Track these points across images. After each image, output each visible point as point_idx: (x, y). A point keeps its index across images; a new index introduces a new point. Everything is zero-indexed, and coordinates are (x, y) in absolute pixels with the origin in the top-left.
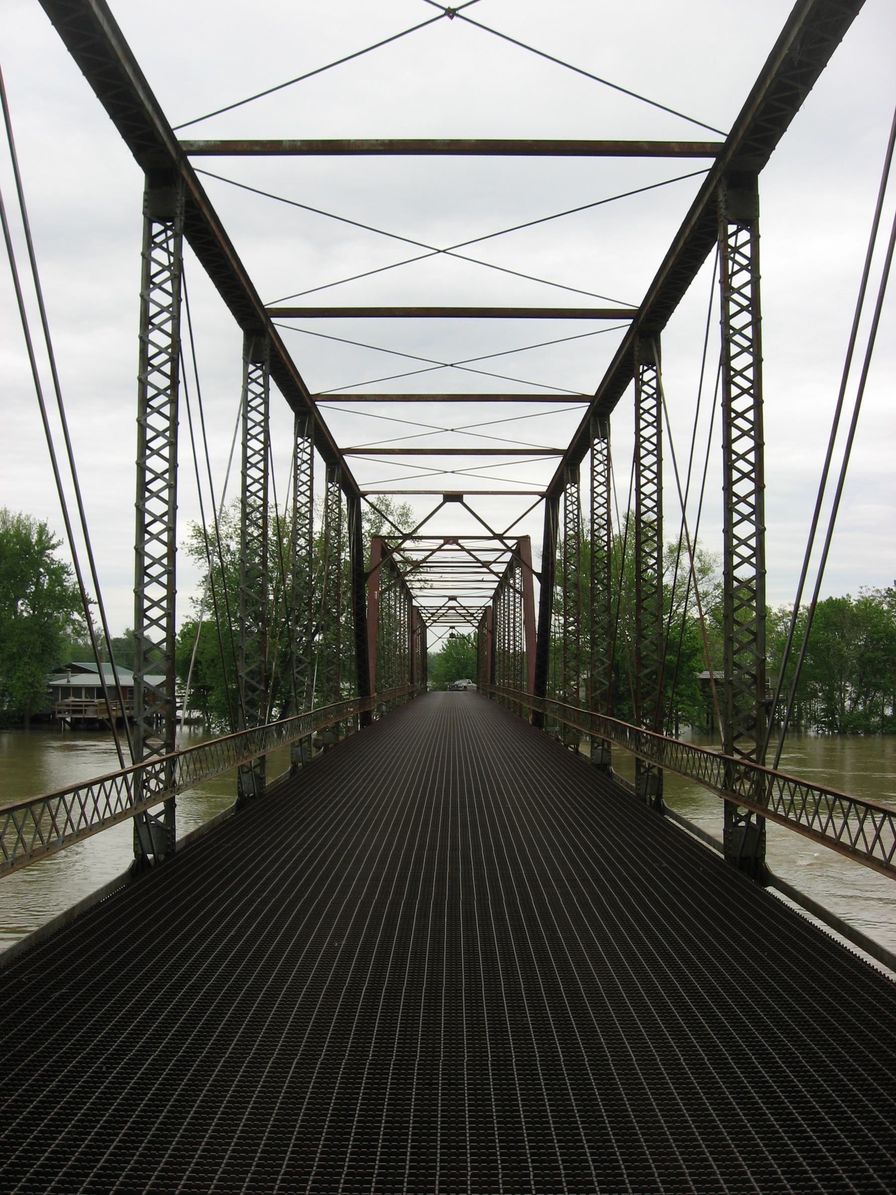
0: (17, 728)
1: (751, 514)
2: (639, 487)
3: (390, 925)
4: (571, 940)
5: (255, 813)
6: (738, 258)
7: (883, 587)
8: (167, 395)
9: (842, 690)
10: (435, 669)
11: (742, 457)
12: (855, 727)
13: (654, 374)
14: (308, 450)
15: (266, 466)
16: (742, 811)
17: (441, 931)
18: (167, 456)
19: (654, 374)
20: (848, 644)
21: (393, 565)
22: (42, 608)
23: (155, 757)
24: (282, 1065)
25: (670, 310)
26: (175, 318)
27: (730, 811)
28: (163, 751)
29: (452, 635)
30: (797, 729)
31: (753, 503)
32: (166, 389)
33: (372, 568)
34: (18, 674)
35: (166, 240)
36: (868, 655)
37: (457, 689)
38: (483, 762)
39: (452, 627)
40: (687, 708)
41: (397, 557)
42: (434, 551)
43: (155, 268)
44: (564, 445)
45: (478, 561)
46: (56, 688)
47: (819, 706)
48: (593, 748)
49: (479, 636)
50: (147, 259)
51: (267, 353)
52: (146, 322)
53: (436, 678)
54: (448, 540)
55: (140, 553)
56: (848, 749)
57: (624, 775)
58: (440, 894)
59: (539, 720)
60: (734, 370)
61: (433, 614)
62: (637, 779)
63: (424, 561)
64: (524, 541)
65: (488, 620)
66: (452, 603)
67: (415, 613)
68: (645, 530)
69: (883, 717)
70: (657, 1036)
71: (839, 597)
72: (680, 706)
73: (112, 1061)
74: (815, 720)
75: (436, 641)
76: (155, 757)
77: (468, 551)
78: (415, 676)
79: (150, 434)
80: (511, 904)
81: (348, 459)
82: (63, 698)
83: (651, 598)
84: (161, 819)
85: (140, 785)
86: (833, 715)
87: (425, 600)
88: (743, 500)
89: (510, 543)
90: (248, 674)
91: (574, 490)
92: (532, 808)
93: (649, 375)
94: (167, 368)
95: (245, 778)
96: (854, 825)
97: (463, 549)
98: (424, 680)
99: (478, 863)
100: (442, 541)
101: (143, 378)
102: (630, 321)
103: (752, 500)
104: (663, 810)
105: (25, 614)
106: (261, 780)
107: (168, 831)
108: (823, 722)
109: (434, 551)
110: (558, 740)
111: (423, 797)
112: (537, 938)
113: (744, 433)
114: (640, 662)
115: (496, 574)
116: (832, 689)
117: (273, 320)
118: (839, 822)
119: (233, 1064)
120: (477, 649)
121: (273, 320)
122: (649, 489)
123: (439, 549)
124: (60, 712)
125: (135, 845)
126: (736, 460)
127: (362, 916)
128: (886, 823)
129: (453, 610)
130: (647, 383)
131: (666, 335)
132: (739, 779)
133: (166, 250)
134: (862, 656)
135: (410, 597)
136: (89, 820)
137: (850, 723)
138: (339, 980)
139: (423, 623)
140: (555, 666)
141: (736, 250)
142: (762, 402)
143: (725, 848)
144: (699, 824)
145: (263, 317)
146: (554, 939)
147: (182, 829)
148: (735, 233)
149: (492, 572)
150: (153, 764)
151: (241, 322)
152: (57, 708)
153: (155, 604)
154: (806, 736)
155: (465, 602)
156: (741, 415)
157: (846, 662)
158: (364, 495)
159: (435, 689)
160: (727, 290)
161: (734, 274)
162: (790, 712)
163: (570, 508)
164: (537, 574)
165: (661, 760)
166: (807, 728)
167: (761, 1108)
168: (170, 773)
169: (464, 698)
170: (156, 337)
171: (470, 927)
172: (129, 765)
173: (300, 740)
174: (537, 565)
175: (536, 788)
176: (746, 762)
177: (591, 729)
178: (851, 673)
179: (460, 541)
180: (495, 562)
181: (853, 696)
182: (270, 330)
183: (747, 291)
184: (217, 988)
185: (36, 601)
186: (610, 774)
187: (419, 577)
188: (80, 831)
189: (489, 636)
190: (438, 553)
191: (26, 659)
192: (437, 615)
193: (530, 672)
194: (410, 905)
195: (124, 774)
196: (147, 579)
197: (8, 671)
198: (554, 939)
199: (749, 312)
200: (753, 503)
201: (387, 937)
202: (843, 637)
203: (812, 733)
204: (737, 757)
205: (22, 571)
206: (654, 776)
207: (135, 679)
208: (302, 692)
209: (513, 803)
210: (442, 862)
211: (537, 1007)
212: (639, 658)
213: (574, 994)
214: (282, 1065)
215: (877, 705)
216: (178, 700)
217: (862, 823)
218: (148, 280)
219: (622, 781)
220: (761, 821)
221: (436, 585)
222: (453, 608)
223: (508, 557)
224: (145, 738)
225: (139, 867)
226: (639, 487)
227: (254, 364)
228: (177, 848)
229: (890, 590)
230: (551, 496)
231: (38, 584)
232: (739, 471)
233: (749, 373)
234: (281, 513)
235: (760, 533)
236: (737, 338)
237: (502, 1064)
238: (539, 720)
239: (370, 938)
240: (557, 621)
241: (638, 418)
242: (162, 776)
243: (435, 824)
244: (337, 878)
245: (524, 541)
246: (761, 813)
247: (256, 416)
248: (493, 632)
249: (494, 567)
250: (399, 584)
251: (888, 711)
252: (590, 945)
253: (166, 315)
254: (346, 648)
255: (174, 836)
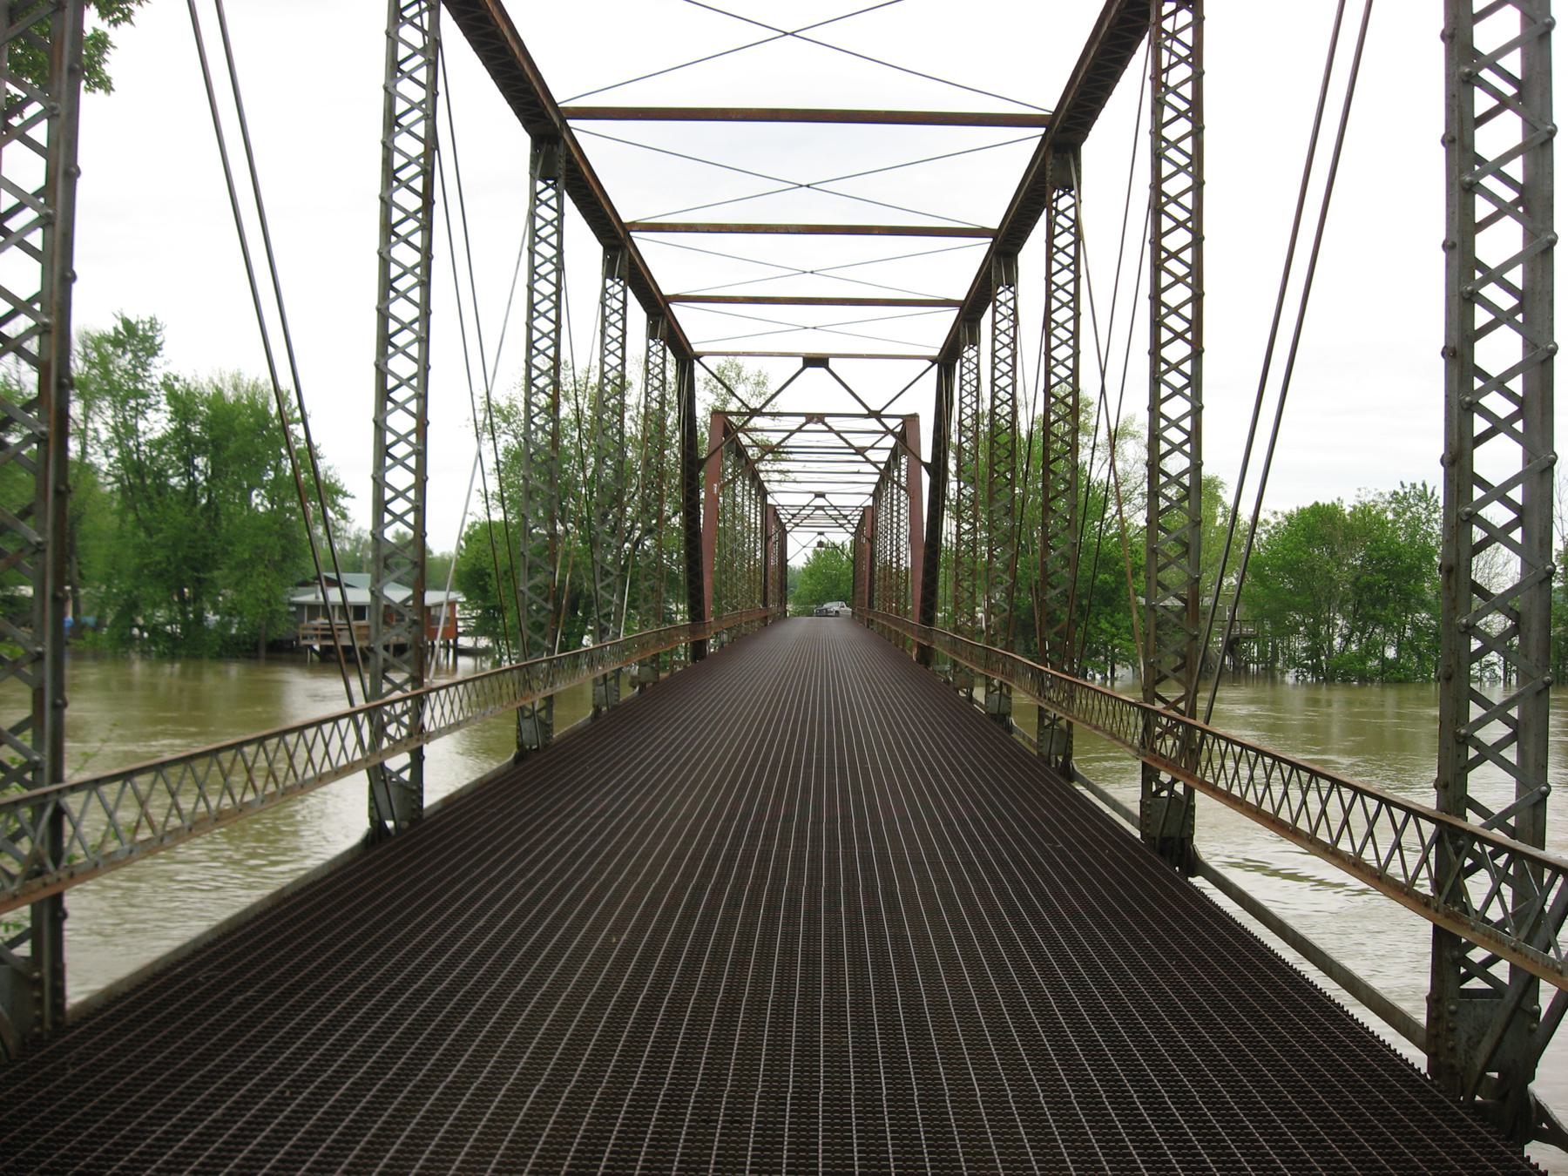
0: (250, 657)
1: (1185, 386)
2: (1048, 350)
3: (688, 917)
4: (921, 940)
5: (536, 773)
6: (1177, 47)
7: (1387, 490)
8: (417, 220)
9: (1330, 623)
10: (797, 588)
11: (1175, 311)
12: (1346, 673)
13: (1072, 201)
14: (620, 296)
15: (558, 316)
16: (1165, 777)
17: (754, 924)
18: (417, 300)
19: (1072, 201)
20: (1339, 565)
21: (740, 451)
22: (283, 501)
23: (398, 694)
24: (518, 1093)
25: (1092, 115)
26: (430, 118)
27: (1149, 775)
28: (409, 687)
29: (820, 544)
30: (1270, 674)
31: (1189, 372)
32: (416, 212)
33: (711, 456)
34: (250, 588)
35: (420, 14)
36: (1365, 578)
37: (826, 614)
38: (844, 708)
39: (821, 534)
40: (1125, 644)
41: (745, 440)
42: (792, 433)
43: (403, 51)
44: (961, 294)
45: (851, 446)
46: (300, 606)
47: (1299, 644)
48: (987, 692)
49: (856, 544)
50: (393, 39)
51: (561, 166)
52: (392, 122)
53: (798, 600)
54: (811, 418)
55: (380, 427)
56: (1336, 698)
57: (1024, 726)
58: (760, 877)
59: (926, 655)
60: (1167, 196)
61: (794, 516)
62: (1039, 734)
63: (779, 445)
64: (911, 421)
65: (868, 525)
66: (820, 502)
67: (770, 514)
68: (1066, 408)
69: (1383, 660)
70: (1013, 1065)
71: (1328, 502)
72: (1116, 642)
73: (298, 1086)
74: (1292, 661)
75: (800, 550)
76: (398, 694)
77: (838, 433)
78: (770, 595)
79: (395, 271)
80: (851, 893)
81: (677, 309)
82: (310, 619)
83: (1085, 502)
84: (406, 775)
85: (379, 731)
86: (1318, 657)
87: (783, 497)
88: (1175, 367)
89: (892, 423)
90: (530, 589)
91: (972, 353)
92: (898, 769)
93: (1065, 202)
94: (418, 184)
95: (526, 724)
96: (1295, 794)
97: (831, 430)
98: (783, 601)
99: (816, 839)
100: (803, 420)
101: (386, 196)
102: (1042, 130)
103: (1187, 367)
104: (1069, 774)
105: (261, 509)
106: (546, 727)
107: (414, 792)
108: (1305, 666)
109: (792, 433)
110: (947, 682)
111: (758, 752)
112: (877, 937)
113: (1178, 280)
114: (1046, 580)
115: (874, 464)
116: (1318, 622)
117: (571, 123)
118: (1277, 790)
119: (455, 1090)
120: (854, 562)
121: (571, 123)
122: (1062, 353)
123: (799, 430)
124: (305, 638)
125: (371, 808)
126: (1167, 315)
127: (653, 903)
128: (1335, 794)
129: (821, 510)
130: (1062, 213)
131: (1088, 149)
132: (1160, 735)
133: (421, 28)
134: (1358, 579)
135: (763, 493)
136: (300, 772)
137: (1339, 667)
138: (609, 985)
139: (782, 526)
140: (945, 588)
141: (1173, 36)
142: (1203, 238)
143: (1143, 822)
144: (1111, 790)
145: (555, 119)
146: (899, 939)
147: (434, 793)
148: (1174, 13)
149: (868, 461)
150: (392, 703)
151: (527, 125)
152: (301, 632)
153: (400, 494)
154: (1283, 682)
155: (836, 500)
156: (1174, 255)
157: (1336, 587)
158: (698, 357)
159: (799, 614)
160: (1160, 88)
161: (1171, 67)
162: (1262, 653)
163: (966, 378)
164: (926, 465)
165: (1068, 711)
166: (1283, 673)
167: (1204, 1162)
168: (417, 715)
169: (835, 627)
170: (403, 141)
171: (791, 920)
172: (360, 702)
173: (605, 676)
174: (926, 456)
175: (908, 744)
176: (1172, 713)
177: (986, 667)
178: (1344, 602)
179: (827, 420)
180: (872, 447)
181: (1345, 631)
182: (566, 136)
183: (1187, 91)
184: (450, 992)
185: (275, 491)
186: (1009, 729)
187: (778, 466)
188: (286, 788)
189: (868, 546)
190: (797, 435)
191: (261, 568)
192: (801, 516)
193: (915, 591)
194: (718, 891)
195: (352, 716)
196: (389, 461)
197: (237, 584)
198: (899, 939)
199: (1187, 118)
200: (1189, 372)
201: (682, 933)
202: (1332, 554)
203: (1290, 678)
204: (1159, 706)
205: (257, 452)
206: (1061, 730)
207: (372, 593)
208: (608, 614)
209: (874, 763)
210: (769, 837)
211: (863, 1026)
212: (1045, 575)
213: (913, 1009)
214: (518, 1093)
215: (1375, 645)
216: (460, 623)
217: (1305, 794)
218: (394, 67)
219: (1024, 737)
220: (1189, 792)
221: (800, 477)
222: (818, 508)
223: (890, 441)
224: (385, 670)
225: (376, 835)
226: (1048, 350)
227: (544, 180)
228: (425, 815)
229: (1396, 493)
230: (947, 360)
231: (277, 469)
232: (1170, 329)
233: (1187, 200)
234: (580, 374)
235: (1196, 412)
236: (1171, 153)
237: (805, 1098)
238: (926, 655)
239: (660, 931)
240: (949, 526)
241: (1050, 259)
242: (406, 719)
243: (768, 788)
244: (629, 854)
245: (911, 421)
246: (1190, 783)
247: (546, 250)
248: (872, 540)
249: (870, 454)
250: (749, 474)
251: (1391, 653)
252: (945, 945)
253: (417, 114)
254: (674, 561)
255: (421, 799)
